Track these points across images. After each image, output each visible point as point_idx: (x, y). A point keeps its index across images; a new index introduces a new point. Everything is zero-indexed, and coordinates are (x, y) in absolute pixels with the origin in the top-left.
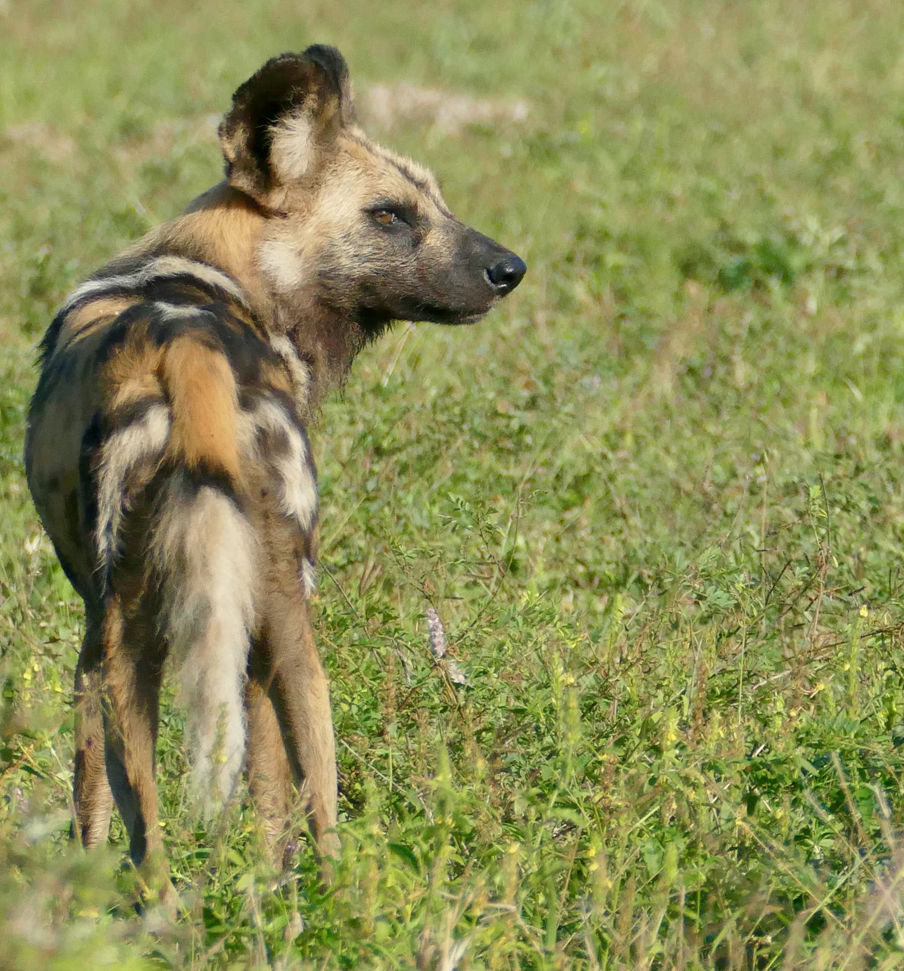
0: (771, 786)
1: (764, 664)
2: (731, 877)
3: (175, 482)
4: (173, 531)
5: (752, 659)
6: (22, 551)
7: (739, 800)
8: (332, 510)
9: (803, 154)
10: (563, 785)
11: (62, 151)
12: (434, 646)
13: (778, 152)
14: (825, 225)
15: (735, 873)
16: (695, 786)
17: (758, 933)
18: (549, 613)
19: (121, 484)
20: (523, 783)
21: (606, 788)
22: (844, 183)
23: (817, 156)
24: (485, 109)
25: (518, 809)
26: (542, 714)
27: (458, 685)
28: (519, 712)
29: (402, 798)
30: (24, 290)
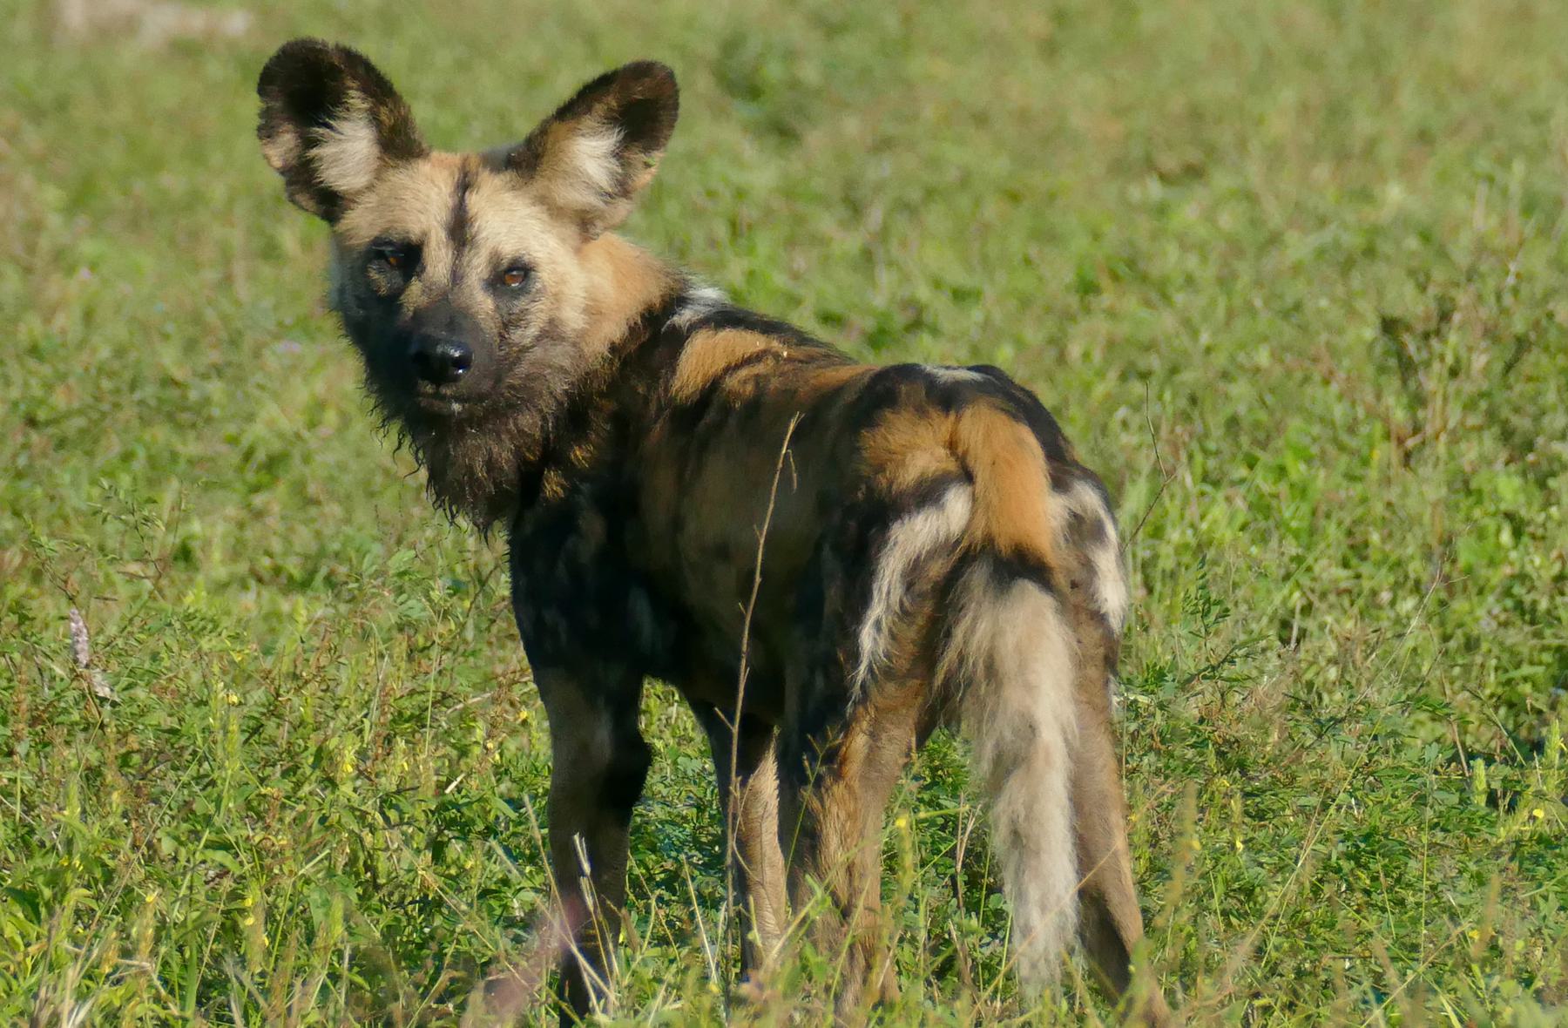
0: (464, 829)
1: (461, 684)
2: (411, 934)
3: (978, 576)
4: (983, 627)
5: (446, 680)
7: (422, 846)
10: (218, 821)
12: (76, 653)
15: (415, 930)
16: (373, 829)
17: (441, 1000)
18: (212, 621)
19: (904, 575)
20: (173, 817)
21: (267, 828)
25: (167, 846)
26: (199, 736)
27: (103, 700)
28: (173, 731)
29: (32, 831)
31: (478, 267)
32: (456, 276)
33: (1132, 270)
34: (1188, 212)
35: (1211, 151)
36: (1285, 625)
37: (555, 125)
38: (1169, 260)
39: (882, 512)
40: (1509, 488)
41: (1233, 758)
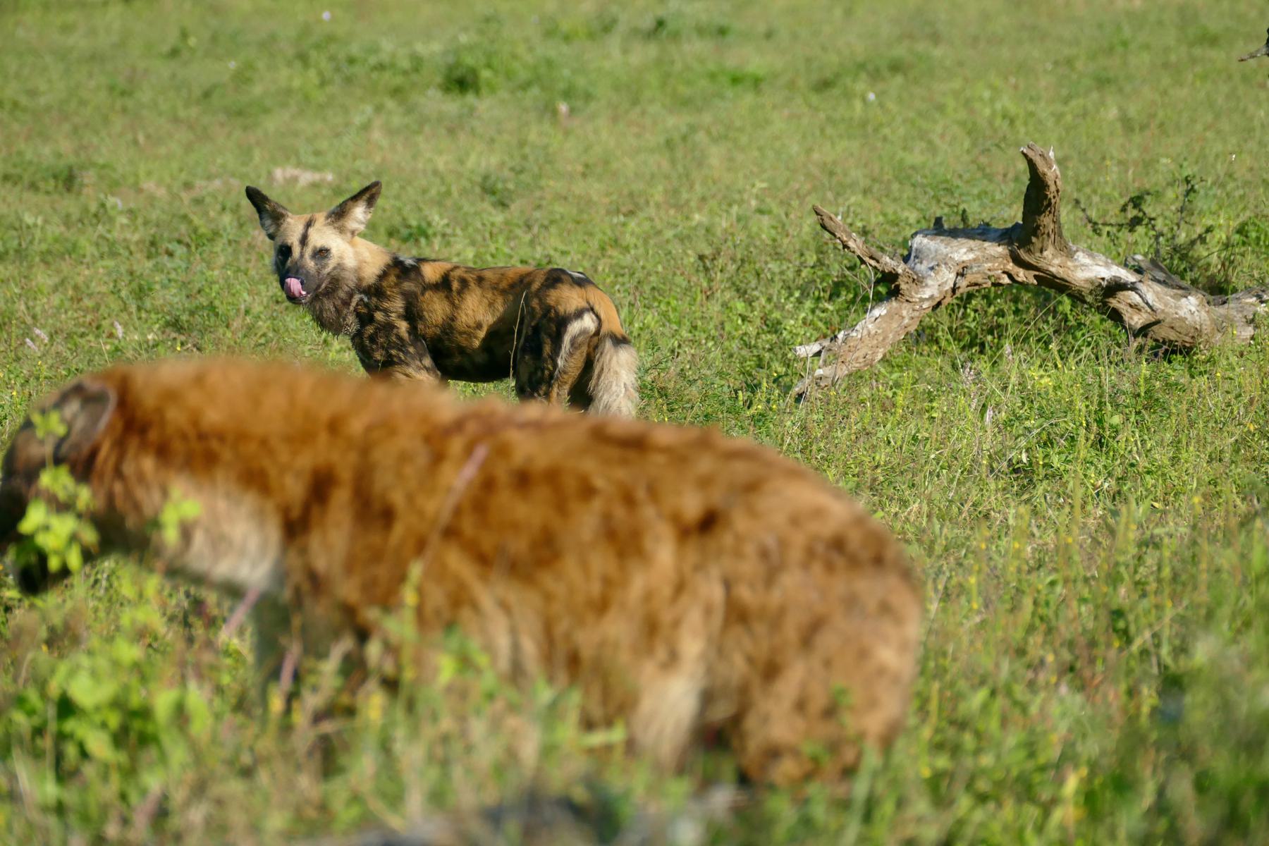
6: (1089, 299)
8: (260, 323)
9: (433, 192)
11: (161, 192)
13: (424, 191)
14: (442, 218)
22: (449, 203)
23: (439, 193)
24: (317, 177)
30: (147, 243)
31: (308, 252)
32: (302, 256)
33: (616, 243)
34: (632, 224)
35: (637, 205)
36: (673, 351)
37: (350, 203)
38: (629, 239)
39: (562, 323)
40: (740, 306)
41: (663, 392)
